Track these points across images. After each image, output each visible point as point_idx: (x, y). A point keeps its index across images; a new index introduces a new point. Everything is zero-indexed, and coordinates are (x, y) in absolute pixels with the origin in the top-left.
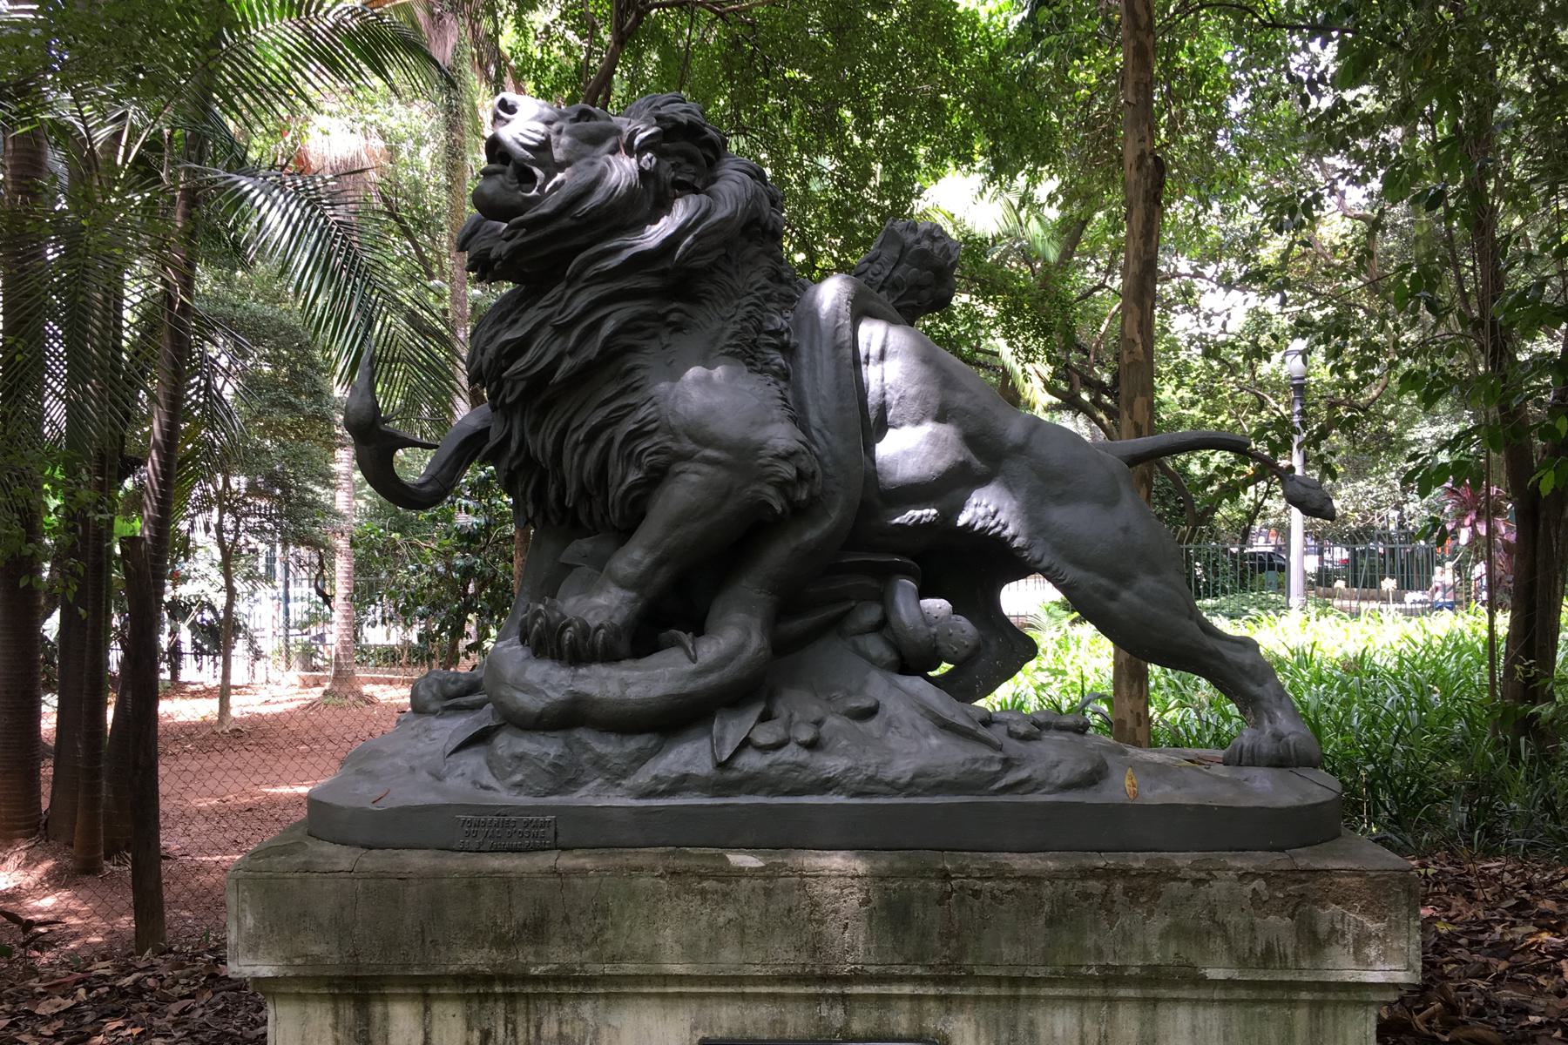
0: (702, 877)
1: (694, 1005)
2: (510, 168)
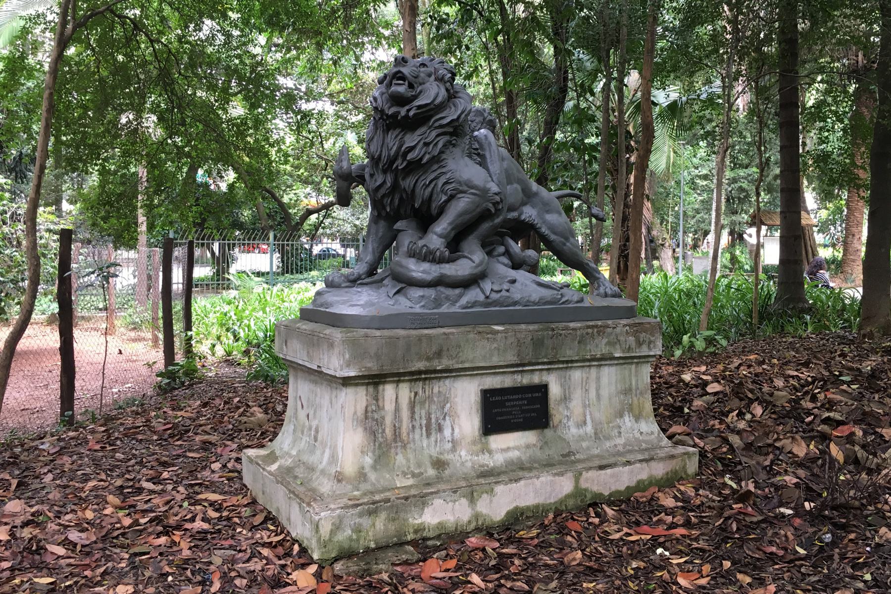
0: (488, 333)
1: (479, 377)
2: (407, 83)
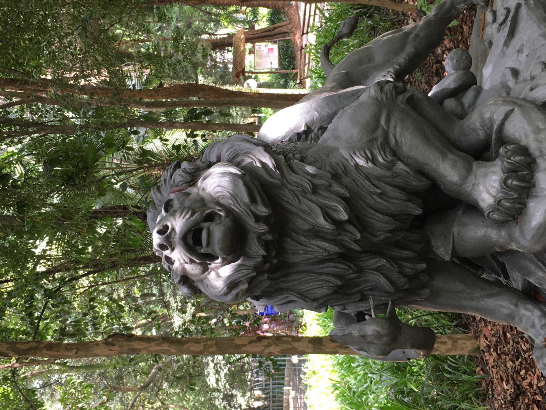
2: (206, 224)
